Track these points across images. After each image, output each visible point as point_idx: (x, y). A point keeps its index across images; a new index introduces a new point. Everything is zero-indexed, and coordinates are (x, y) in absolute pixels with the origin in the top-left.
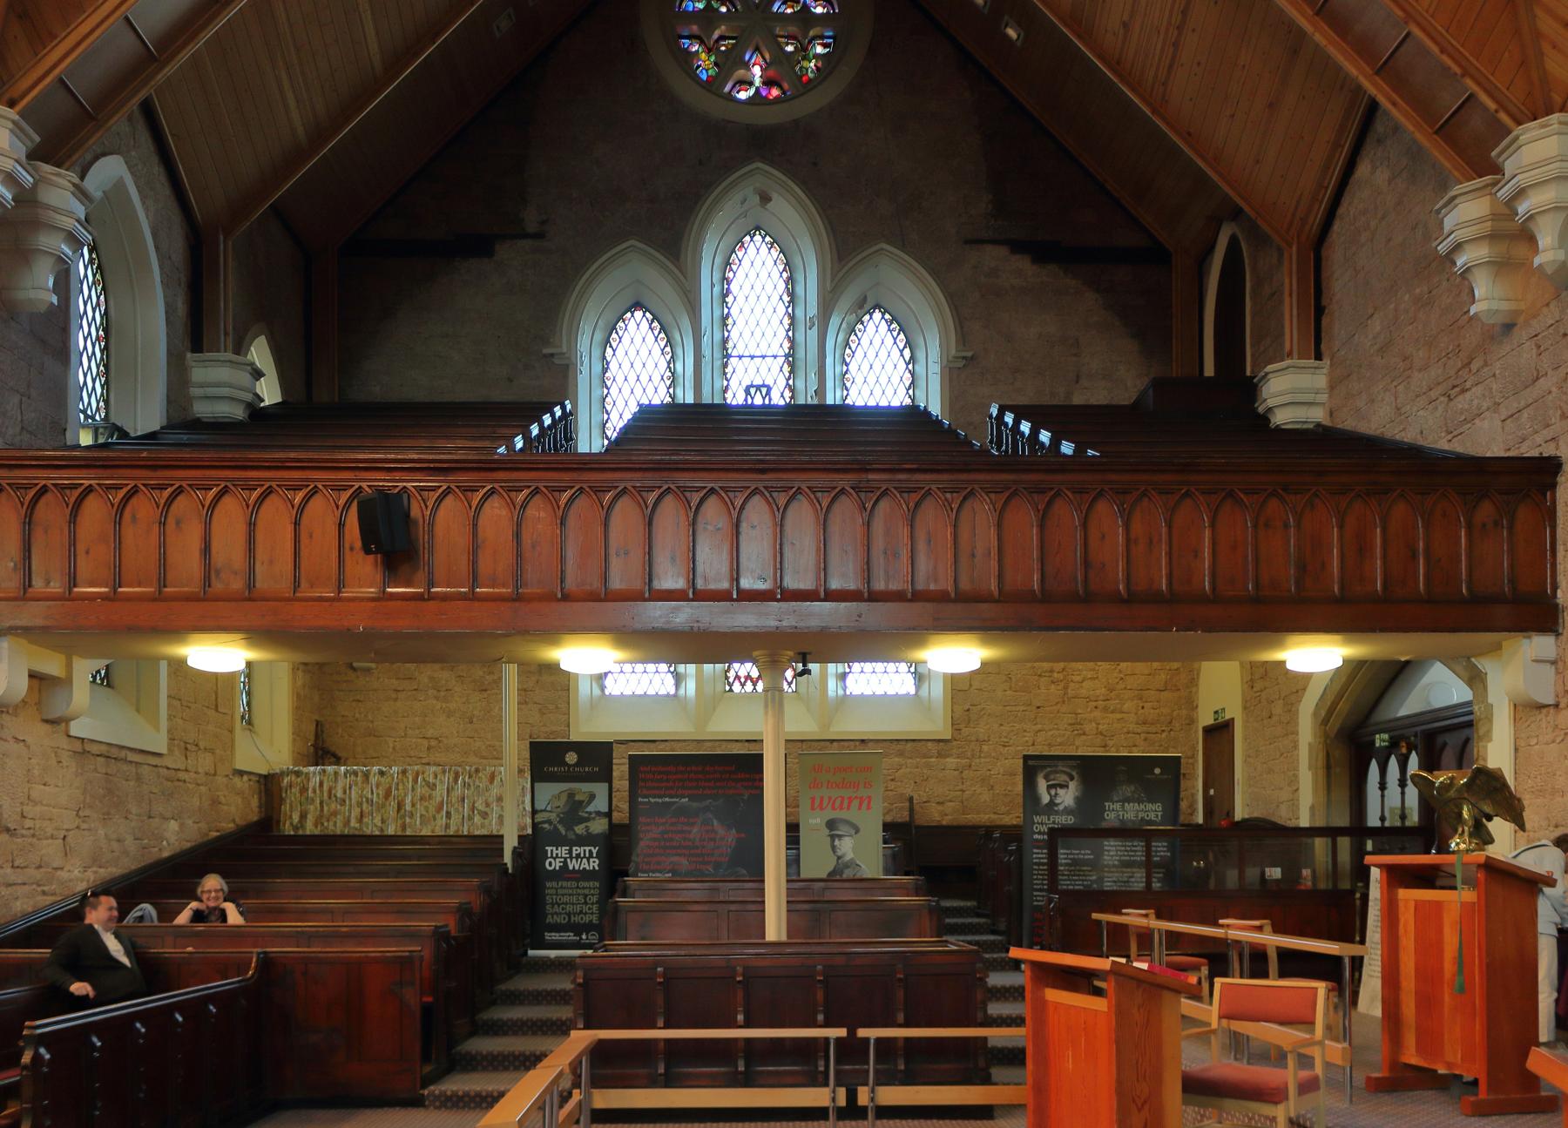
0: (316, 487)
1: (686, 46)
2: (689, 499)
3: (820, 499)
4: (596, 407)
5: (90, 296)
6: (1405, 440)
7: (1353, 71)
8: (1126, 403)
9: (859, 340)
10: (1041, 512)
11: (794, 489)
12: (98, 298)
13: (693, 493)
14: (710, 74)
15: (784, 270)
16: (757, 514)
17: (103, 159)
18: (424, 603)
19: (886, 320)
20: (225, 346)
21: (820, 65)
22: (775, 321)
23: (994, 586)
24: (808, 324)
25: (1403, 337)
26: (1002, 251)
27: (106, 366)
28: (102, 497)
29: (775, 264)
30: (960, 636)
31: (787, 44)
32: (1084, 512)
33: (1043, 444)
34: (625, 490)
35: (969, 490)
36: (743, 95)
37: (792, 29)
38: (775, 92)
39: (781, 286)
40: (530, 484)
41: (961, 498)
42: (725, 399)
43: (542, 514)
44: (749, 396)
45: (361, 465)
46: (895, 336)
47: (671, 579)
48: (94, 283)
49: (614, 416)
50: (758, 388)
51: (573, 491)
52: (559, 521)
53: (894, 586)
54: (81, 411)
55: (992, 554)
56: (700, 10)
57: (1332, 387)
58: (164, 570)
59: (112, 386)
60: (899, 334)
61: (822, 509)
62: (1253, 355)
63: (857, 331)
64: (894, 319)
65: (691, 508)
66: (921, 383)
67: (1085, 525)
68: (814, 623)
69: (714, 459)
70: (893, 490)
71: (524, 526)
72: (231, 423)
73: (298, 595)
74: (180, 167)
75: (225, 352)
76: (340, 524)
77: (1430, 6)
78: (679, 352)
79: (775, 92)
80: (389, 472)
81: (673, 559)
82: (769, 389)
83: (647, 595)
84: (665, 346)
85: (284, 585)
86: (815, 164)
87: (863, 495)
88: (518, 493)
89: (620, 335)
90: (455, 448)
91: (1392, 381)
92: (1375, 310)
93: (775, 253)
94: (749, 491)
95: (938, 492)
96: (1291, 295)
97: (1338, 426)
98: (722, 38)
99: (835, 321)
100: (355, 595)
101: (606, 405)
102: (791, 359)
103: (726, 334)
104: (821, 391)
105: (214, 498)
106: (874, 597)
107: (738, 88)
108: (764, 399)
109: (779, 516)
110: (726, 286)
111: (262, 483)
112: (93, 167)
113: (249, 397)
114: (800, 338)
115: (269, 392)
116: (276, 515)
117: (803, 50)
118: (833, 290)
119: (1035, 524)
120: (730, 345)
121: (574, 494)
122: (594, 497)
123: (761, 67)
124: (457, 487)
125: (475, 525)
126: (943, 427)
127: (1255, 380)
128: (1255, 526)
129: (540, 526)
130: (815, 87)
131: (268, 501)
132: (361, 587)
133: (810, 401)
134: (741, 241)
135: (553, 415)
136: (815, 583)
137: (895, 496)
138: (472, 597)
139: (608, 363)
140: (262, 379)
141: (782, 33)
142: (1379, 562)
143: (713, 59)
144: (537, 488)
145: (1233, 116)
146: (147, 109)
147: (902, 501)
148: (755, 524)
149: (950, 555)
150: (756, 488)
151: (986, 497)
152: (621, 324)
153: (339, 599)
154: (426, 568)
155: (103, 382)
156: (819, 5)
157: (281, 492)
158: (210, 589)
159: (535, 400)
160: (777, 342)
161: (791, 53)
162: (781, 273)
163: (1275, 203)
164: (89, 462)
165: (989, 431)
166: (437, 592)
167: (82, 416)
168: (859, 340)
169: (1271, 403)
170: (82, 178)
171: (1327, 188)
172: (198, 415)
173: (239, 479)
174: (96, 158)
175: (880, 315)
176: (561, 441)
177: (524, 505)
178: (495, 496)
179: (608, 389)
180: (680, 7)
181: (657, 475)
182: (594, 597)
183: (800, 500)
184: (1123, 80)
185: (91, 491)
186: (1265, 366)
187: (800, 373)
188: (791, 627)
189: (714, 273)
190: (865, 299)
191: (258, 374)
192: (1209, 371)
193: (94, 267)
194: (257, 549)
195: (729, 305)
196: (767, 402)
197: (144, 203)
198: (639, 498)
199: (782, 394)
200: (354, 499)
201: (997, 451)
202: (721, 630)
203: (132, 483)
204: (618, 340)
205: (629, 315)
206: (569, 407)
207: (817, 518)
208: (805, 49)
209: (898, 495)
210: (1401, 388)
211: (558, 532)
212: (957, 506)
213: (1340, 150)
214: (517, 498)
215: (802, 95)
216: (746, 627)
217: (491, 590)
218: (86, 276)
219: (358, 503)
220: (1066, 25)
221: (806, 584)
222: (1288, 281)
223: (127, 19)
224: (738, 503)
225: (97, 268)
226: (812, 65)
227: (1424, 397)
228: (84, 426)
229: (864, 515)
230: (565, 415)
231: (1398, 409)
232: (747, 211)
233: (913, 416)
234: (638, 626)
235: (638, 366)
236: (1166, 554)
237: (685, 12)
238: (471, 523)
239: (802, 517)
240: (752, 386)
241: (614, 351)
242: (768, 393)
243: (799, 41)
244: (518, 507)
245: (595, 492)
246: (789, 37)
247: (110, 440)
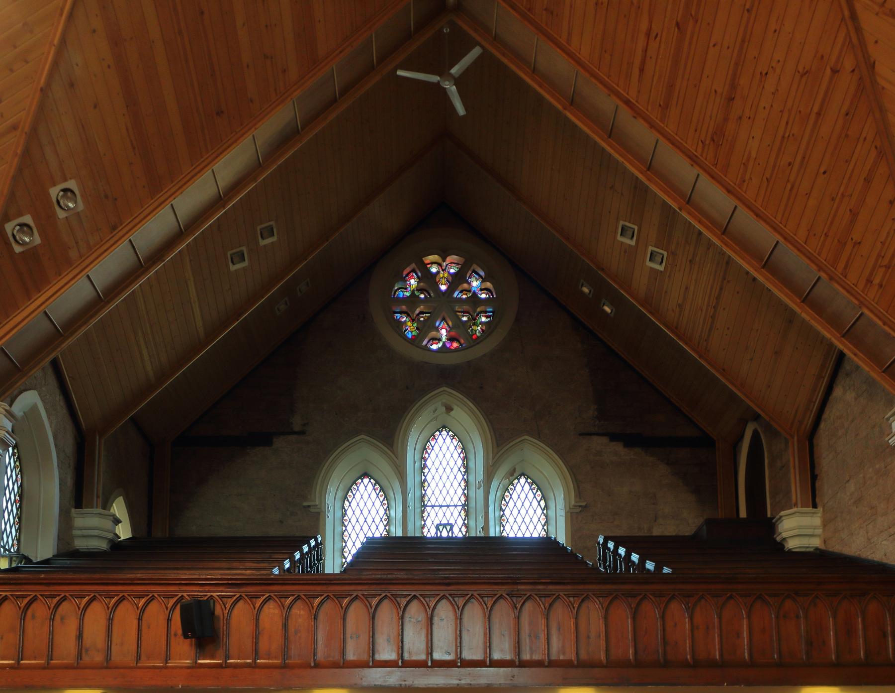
0: (153, 596)
1: (398, 318)
2: (399, 602)
3: (486, 602)
4: (337, 538)
5: (11, 476)
6: (875, 559)
7: (827, 335)
8: (687, 534)
10: (633, 609)
11: (469, 596)
12: (17, 476)
13: (402, 598)
14: (413, 334)
15: (462, 452)
16: (444, 613)
17: (25, 392)
18: (222, 670)
19: (529, 483)
20: (97, 506)
21: (484, 328)
22: (456, 484)
23: (603, 657)
24: (477, 486)
25: (870, 495)
26: (604, 440)
27: (19, 518)
28: (13, 603)
29: (456, 449)
30: (581, 689)
31: (463, 316)
32: (662, 609)
33: (634, 562)
34: (357, 597)
35: (585, 595)
36: (434, 347)
37: (466, 307)
38: (455, 345)
39: (460, 462)
40: (295, 593)
41: (580, 601)
42: (423, 533)
43: (302, 612)
44: (438, 531)
45: (183, 582)
46: (535, 493)
47: (386, 653)
48: (14, 467)
49: (350, 544)
50: (445, 526)
51: (323, 597)
52: (313, 617)
53: (536, 657)
54: (2, 547)
55: (601, 636)
56: (408, 297)
57: (825, 524)
58: (52, 649)
59: (23, 530)
60: (537, 491)
61: (487, 608)
62: (771, 504)
63: (510, 490)
64: (534, 482)
65: (400, 608)
66: (552, 522)
67: (663, 617)
68: (483, 681)
69: (416, 577)
70: (534, 596)
71: (290, 621)
72: (97, 552)
73: (139, 665)
74: (74, 396)
75: (97, 508)
76: (168, 619)
77: (875, 297)
78: (393, 504)
79: (455, 345)
80: (201, 586)
81: (388, 641)
82: (452, 526)
83: (371, 664)
85: (130, 660)
86: (481, 388)
87: (514, 599)
88: (286, 599)
89: (354, 493)
90: (244, 570)
91: (864, 522)
92: (850, 477)
93: (455, 442)
94: (439, 597)
95: (565, 597)
96: (794, 468)
97: (830, 550)
98: (421, 313)
99: (495, 484)
100: (176, 665)
101: (344, 537)
102: (466, 507)
103: (423, 492)
104: (486, 528)
105: (86, 603)
106: (523, 664)
107: (431, 342)
108: (448, 532)
109: (459, 613)
110: (423, 463)
111: (118, 593)
112: (19, 397)
113: (111, 536)
114: (472, 494)
115: (124, 532)
116: (126, 614)
117: (473, 320)
118: (493, 465)
119: (629, 617)
120: (426, 499)
121: (323, 599)
122: (337, 601)
123: (446, 330)
124: (246, 595)
125: (257, 620)
126: (567, 552)
127: (774, 521)
128: (777, 617)
129: (300, 620)
130: (481, 342)
131: (121, 606)
132: (181, 660)
133: (479, 535)
134: (433, 435)
135: (309, 545)
136: (483, 656)
137: (536, 599)
138: (253, 666)
139: (346, 511)
140: (120, 524)
141: (460, 310)
142: (861, 640)
143: (415, 325)
144: (299, 596)
145: (751, 359)
146: (55, 364)
147: (541, 603)
148: (443, 618)
149: (573, 637)
150: (444, 595)
151: (597, 600)
152: (354, 486)
153: (166, 668)
154: (224, 647)
155: (18, 506)
156: (483, 293)
157: (130, 599)
158: (82, 661)
159: (297, 534)
160: (457, 497)
161: (466, 321)
162: (459, 454)
163: (781, 412)
164: (6, 581)
165: (598, 552)
166: (231, 663)
167: (2, 550)
169: (784, 535)
170: (11, 405)
171: (815, 402)
172: (78, 548)
173: (104, 591)
174: (21, 393)
175: (524, 480)
176: (314, 561)
177: (290, 607)
178: (271, 601)
179: (346, 543)
180: (394, 295)
181: (379, 587)
182: (336, 665)
183: (473, 602)
184: (680, 338)
185: (6, 599)
186: (780, 511)
187: (472, 516)
188: (468, 684)
189: (416, 455)
190: (514, 470)
191: (117, 521)
192: (743, 514)
193: (15, 458)
194: (113, 633)
195: (425, 474)
196: (450, 535)
197: (49, 418)
198: (366, 602)
199: (460, 529)
200: (178, 603)
201: (603, 568)
202: (420, 686)
203: (34, 594)
204: (353, 496)
205: (360, 481)
206: (320, 539)
207: (484, 613)
208: (475, 319)
209: (538, 599)
210: (870, 526)
211: (313, 623)
212: (577, 605)
213: (822, 379)
214: (285, 602)
215: (472, 346)
216: (437, 685)
217: (267, 661)
218: (10, 463)
219: (181, 606)
220: (642, 306)
221: (478, 656)
222: (792, 458)
223: (45, 313)
224: (432, 605)
225: (17, 458)
226: (479, 328)
227: (886, 532)
228: (3, 556)
229: (515, 612)
230: (317, 545)
231: (869, 540)
232: (437, 417)
233: (547, 544)
234: (365, 684)
235: (365, 512)
236: (718, 635)
237: (398, 298)
238: (255, 618)
239: (474, 615)
240: (440, 524)
241: (350, 503)
242: (451, 529)
243: (470, 314)
244: (286, 608)
245: (337, 598)
246: (464, 312)
247: (19, 565)
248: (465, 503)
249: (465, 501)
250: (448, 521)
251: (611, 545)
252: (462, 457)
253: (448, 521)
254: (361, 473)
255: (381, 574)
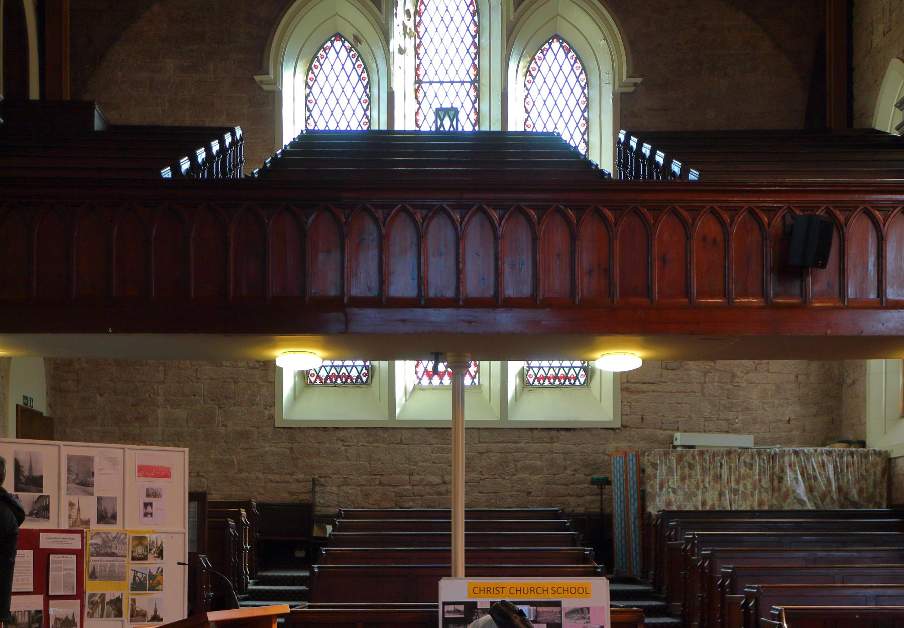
9: (539, 67)
19: (345, 47)
63: (537, 60)
78: (375, 78)
84: (362, 73)
89: (322, 63)
152: (322, 52)
160: (464, 69)
162: (468, 7)
168: (539, 67)
248: (476, 78)
249: (476, 75)
250: (441, 105)
251: (633, 142)
252: (471, 11)
253: (441, 105)
254: (552, 35)
255: (765, 202)
